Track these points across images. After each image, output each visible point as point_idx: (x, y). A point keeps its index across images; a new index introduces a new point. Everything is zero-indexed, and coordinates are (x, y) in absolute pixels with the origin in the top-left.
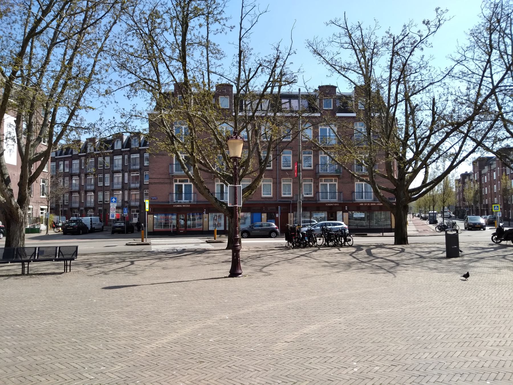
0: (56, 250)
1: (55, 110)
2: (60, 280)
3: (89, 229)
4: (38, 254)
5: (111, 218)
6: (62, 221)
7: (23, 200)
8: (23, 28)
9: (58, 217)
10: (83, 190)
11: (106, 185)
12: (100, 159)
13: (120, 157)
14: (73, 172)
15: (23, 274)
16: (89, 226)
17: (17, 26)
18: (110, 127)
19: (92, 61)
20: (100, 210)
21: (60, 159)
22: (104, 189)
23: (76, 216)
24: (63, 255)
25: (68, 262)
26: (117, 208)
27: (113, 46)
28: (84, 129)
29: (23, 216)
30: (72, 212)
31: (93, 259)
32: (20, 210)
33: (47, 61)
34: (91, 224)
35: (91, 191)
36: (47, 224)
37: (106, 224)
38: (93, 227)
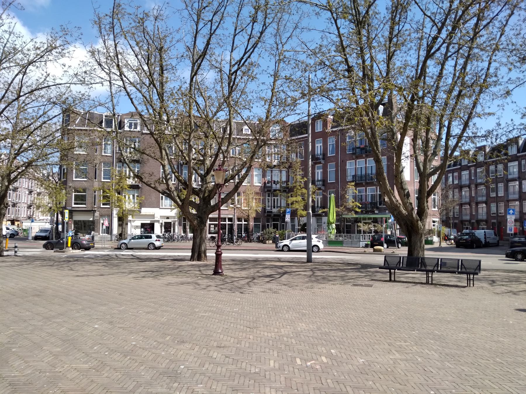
0: (458, 263)
1: (450, 124)
2: (465, 293)
3: (483, 242)
4: (441, 265)
5: (508, 232)
6: (453, 234)
7: (422, 212)
8: (417, 52)
9: (449, 229)
10: (473, 202)
11: (499, 195)
12: (492, 168)
13: (516, 163)
14: (463, 183)
15: (427, 283)
16: (483, 240)
17: (412, 52)
18: (507, 131)
19: (486, 64)
20: (493, 223)
21: (449, 172)
22: (497, 200)
23: (467, 229)
24: (465, 268)
25: (472, 276)
26: (516, 220)
27: (510, 41)
28: (480, 137)
29: (423, 228)
30: (462, 224)
31: (495, 275)
32: (419, 222)
33: (440, 75)
34: (485, 238)
35: (482, 202)
36: (439, 236)
37: (501, 239)
38: (487, 240)
